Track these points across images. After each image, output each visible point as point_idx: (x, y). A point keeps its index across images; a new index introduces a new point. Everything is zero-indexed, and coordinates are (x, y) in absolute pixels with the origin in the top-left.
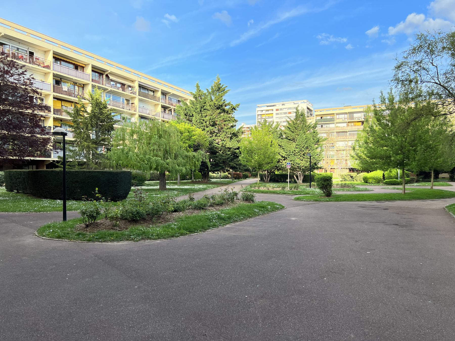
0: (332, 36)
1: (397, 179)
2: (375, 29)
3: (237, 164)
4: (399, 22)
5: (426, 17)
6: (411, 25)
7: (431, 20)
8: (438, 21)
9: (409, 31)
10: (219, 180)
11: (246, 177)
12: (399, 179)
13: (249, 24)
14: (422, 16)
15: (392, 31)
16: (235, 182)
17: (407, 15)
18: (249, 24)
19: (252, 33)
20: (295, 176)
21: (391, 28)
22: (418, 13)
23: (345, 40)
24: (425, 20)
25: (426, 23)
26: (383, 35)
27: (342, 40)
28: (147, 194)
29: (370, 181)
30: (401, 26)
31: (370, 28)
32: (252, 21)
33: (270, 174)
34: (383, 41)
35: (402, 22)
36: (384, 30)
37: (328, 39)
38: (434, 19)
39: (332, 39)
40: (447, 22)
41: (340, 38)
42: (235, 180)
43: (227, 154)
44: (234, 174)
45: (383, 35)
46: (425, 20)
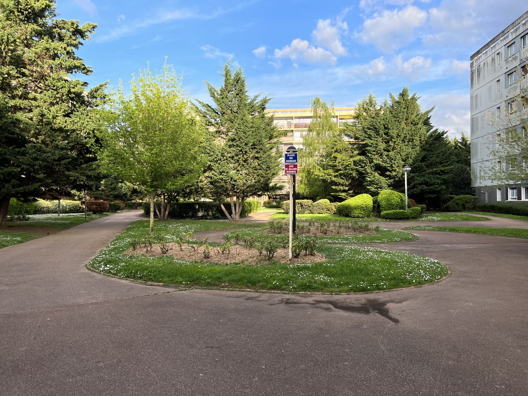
0: (217, 50)
1: (402, 208)
2: (262, 50)
3: (89, 177)
4: (285, 46)
5: (310, 44)
6: (296, 50)
7: (314, 48)
8: (320, 50)
9: (294, 57)
10: (56, 215)
11: (115, 209)
12: (407, 209)
13: (119, 20)
14: (305, 43)
15: (279, 53)
16: (92, 219)
17: (296, 38)
18: (119, 20)
19: (125, 30)
20: (222, 206)
21: (277, 50)
22: (303, 39)
23: (231, 56)
24: (309, 47)
25: (310, 51)
26: (269, 56)
27: (229, 55)
28: (475, 68)
29: (357, 212)
30: (287, 50)
31: (257, 47)
32: (123, 17)
33: (169, 202)
34: (270, 63)
35: (287, 46)
36: (270, 51)
37: (214, 52)
38: (316, 48)
39: (218, 53)
40: (327, 52)
41: (226, 53)
42: (94, 216)
43: (57, 147)
44: (92, 204)
45: (269, 56)
46: (309, 47)
